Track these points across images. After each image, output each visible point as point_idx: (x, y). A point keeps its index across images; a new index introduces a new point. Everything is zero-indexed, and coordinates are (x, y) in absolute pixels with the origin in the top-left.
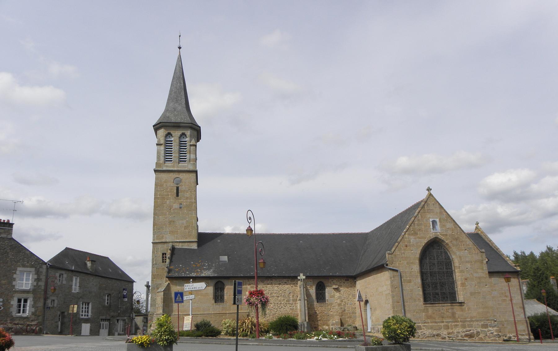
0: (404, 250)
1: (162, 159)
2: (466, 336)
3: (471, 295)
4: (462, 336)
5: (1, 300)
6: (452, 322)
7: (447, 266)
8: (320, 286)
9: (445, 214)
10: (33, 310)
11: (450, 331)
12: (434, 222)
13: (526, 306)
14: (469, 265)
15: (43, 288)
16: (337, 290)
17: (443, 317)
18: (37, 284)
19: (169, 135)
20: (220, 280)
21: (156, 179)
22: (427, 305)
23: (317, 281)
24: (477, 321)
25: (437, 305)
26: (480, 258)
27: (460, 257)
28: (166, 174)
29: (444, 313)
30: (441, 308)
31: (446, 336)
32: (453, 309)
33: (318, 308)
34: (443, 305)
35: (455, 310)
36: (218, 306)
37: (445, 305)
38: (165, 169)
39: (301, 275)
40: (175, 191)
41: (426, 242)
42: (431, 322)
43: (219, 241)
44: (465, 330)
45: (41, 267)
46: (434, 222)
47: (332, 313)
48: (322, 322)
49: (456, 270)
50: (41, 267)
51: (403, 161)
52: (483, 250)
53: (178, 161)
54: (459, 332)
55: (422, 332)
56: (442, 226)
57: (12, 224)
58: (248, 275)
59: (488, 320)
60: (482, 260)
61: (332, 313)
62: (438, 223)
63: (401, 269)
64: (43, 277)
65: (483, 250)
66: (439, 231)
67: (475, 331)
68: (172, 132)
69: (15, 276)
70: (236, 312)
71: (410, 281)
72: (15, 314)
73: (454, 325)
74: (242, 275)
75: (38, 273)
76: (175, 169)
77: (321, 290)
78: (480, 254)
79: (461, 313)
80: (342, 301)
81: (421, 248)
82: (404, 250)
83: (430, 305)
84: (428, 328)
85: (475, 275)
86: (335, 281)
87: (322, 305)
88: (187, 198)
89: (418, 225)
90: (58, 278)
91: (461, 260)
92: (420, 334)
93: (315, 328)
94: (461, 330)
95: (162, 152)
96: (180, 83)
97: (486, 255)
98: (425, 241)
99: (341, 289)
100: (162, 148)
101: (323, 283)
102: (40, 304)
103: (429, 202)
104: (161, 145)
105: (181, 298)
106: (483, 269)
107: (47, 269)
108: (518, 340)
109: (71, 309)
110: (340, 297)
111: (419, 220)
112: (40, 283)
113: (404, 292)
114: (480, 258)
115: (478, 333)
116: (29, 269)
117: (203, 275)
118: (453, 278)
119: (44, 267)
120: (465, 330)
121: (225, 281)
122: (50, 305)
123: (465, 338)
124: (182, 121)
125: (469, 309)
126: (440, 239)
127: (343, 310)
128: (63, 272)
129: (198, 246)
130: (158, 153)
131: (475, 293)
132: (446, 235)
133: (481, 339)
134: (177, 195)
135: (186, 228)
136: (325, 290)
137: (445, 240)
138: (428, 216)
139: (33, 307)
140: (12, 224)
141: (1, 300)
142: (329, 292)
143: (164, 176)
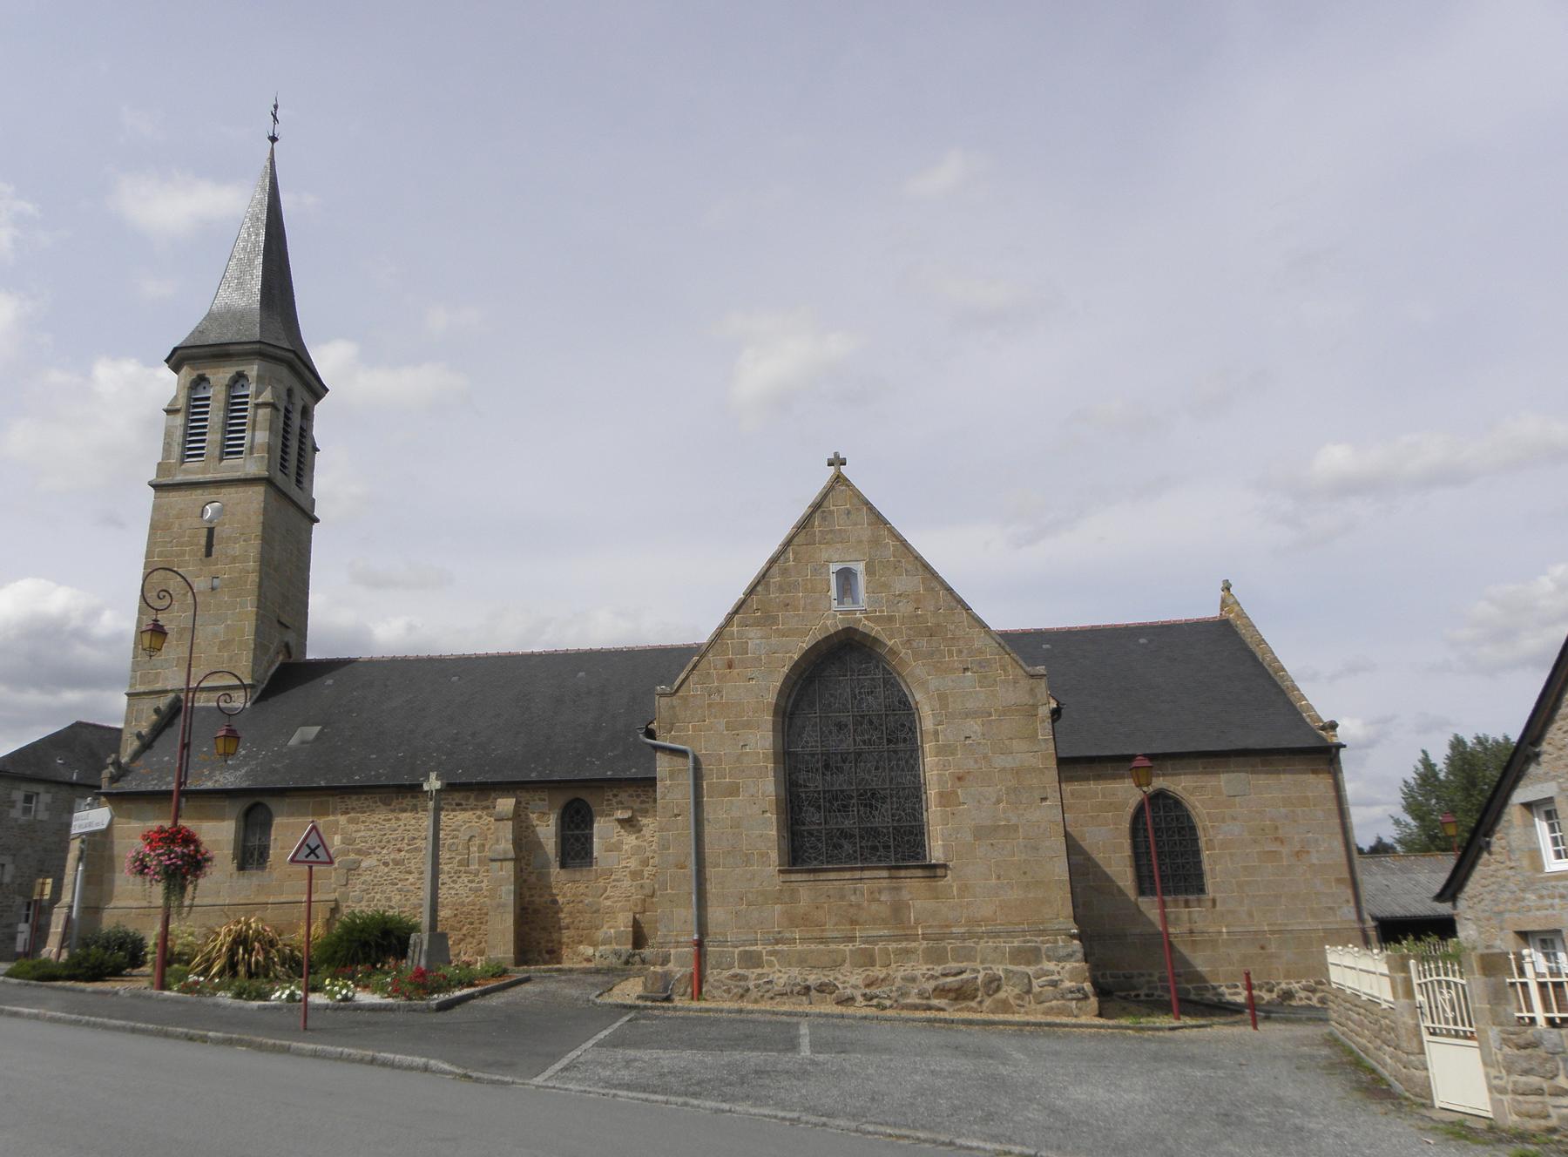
0: (722, 678)
1: (176, 450)
2: (941, 991)
3: (977, 838)
4: (921, 994)
6: (891, 939)
7: (897, 730)
8: (578, 812)
9: (892, 543)
12: (846, 576)
13: (1362, 877)
14: (975, 727)
16: (630, 824)
17: (853, 922)
19: (201, 381)
20: (258, 799)
21: (156, 508)
22: (793, 877)
23: (562, 799)
24: (996, 935)
25: (832, 876)
27: (942, 698)
28: (182, 493)
29: (859, 906)
30: (849, 886)
31: (858, 994)
32: (898, 889)
33: (564, 885)
34: (858, 874)
36: (244, 882)
37: (867, 874)
38: (179, 478)
39: (433, 776)
40: (203, 541)
41: (806, 646)
43: (330, 682)
44: (939, 969)
46: (846, 576)
47: (608, 903)
48: (572, 932)
49: (926, 746)
51: (1336, 458)
52: (1041, 669)
53: (217, 453)
54: (913, 979)
55: (760, 976)
58: (344, 782)
59: (1042, 932)
60: (1035, 706)
61: (608, 903)
62: (862, 580)
63: (700, 747)
65: (1041, 669)
66: (861, 608)
67: (981, 976)
68: (209, 374)
70: (305, 898)
71: (733, 791)
74: (323, 784)
76: (209, 477)
77: (578, 827)
78: (1025, 683)
79: (930, 904)
80: (645, 863)
82: (722, 678)
83: (805, 877)
84: (785, 959)
85: (1000, 761)
86: (623, 796)
87: (578, 876)
88: (234, 559)
89: (781, 589)
90: (20, 805)
92: (751, 985)
93: (551, 952)
94: (922, 969)
95: (179, 433)
96: (257, 235)
97: (1050, 687)
99: (644, 821)
100: (179, 420)
103: (830, 505)
104: (177, 411)
106: (1033, 737)
108: (1252, 1004)
109: (38, 889)
110: (637, 850)
111: (785, 572)
113: (708, 829)
115: (993, 984)
117: (209, 785)
118: (917, 776)
120: (939, 969)
121: (273, 804)
123: (935, 1002)
124: (237, 338)
126: (866, 636)
127: (648, 891)
128: (40, 788)
130: (168, 434)
131: (996, 828)
132: (891, 619)
133: (1004, 1006)
134: (209, 553)
135: (224, 645)
136: (589, 824)
137: (883, 637)
138: (825, 556)
142: (604, 830)
143: (175, 498)
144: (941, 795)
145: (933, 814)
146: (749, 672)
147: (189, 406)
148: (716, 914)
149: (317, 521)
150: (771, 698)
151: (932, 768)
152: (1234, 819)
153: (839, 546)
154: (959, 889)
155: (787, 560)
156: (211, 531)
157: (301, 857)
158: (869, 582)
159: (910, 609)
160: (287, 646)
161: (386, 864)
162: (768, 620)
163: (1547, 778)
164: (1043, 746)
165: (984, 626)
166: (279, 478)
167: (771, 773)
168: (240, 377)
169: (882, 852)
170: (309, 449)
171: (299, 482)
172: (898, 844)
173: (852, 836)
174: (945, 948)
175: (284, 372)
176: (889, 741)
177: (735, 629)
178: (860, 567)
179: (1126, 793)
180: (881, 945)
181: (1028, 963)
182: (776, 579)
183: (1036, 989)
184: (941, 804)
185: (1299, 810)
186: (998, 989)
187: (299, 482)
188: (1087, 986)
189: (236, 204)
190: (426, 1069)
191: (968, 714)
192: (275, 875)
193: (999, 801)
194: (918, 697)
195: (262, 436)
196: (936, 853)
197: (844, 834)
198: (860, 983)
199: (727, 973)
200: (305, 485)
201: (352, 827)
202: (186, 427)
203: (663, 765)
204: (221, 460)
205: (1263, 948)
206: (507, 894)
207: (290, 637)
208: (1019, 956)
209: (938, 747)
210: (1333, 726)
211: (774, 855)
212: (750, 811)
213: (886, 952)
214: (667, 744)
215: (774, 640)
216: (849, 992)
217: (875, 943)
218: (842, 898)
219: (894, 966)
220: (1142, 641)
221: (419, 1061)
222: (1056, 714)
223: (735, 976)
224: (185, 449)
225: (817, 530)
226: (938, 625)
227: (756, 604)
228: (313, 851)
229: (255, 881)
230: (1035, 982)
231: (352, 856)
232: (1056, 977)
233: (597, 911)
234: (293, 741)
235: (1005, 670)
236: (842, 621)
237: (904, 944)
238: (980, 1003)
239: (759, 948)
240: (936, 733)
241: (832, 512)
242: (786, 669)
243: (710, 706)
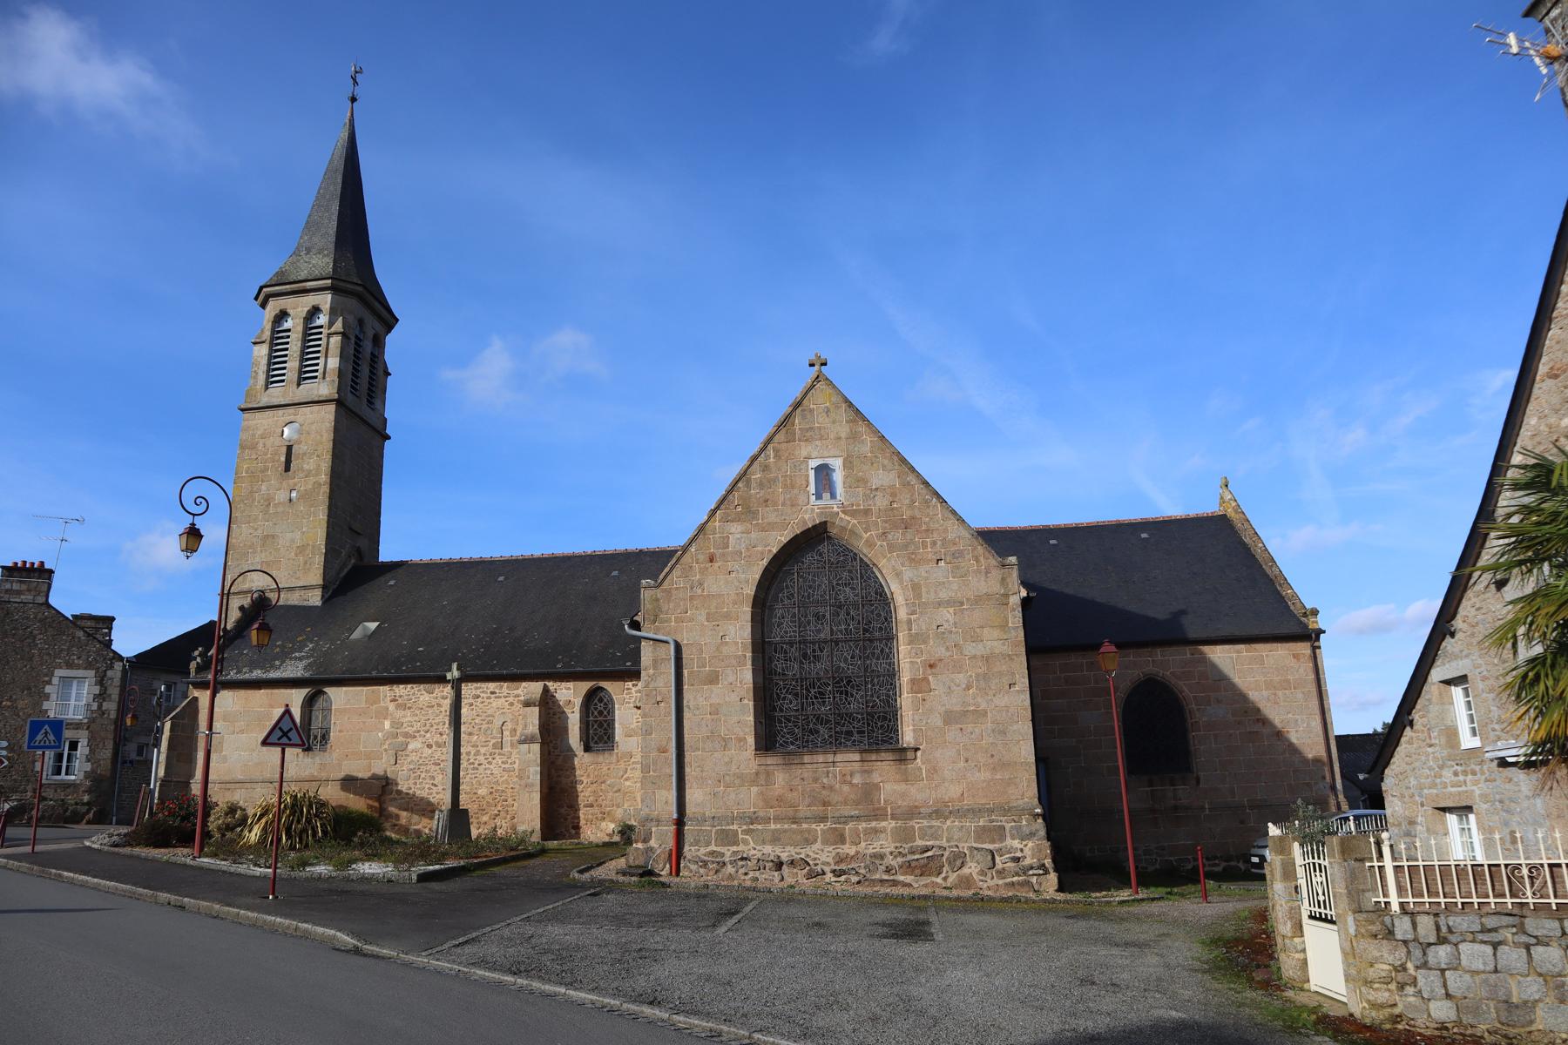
5: (5, 744)
10: (88, 767)
12: (823, 472)
14: (947, 615)
15: (113, 715)
18: (100, 707)
27: (916, 587)
29: (831, 788)
32: (869, 772)
35: (876, 778)
40: (283, 459)
41: (785, 540)
42: (777, 819)
45: (111, 667)
50: (111, 667)
52: (1013, 559)
54: (882, 857)
56: (854, 481)
57: (51, 572)
60: (1006, 596)
62: (838, 477)
64: (114, 692)
66: (837, 505)
67: (946, 854)
69: (48, 689)
71: (713, 679)
72: (47, 776)
73: (867, 832)
75: (101, 681)
78: (996, 574)
79: (902, 787)
81: (765, 563)
85: (971, 649)
87: (600, 758)
89: (761, 485)
91: (919, 596)
102: (106, 754)
105: (52, 737)
107: (124, 671)
111: (766, 468)
112: (105, 706)
113: (687, 715)
119: (118, 666)
122: (133, 756)
125: (933, 770)
129: (326, 600)
132: (867, 512)
134: (287, 469)
138: (804, 453)
140: (51, 572)
141: (5, 744)
144: (913, 681)
145: (906, 701)
147: (272, 339)
148: (694, 795)
152: (1219, 702)
154: (928, 771)
155: (768, 457)
156: (289, 448)
157: (273, 739)
158: (846, 477)
160: (359, 551)
161: (430, 746)
162: (749, 513)
163: (1455, 657)
164: (1013, 633)
165: (961, 520)
168: (315, 311)
169: (856, 737)
170: (381, 373)
171: (370, 403)
172: (876, 730)
173: (828, 721)
175: (352, 303)
176: (865, 631)
180: (850, 825)
182: (756, 476)
183: (999, 866)
184: (912, 691)
186: (963, 864)
187: (370, 403)
188: (1048, 862)
189: (323, 155)
190: (357, 951)
191: (940, 604)
192: (335, 755)
195: (333, 363)
197: (820, 720)
198: (830, 860)
199: (703, 850)
201: (400, 713)
203: (647, 653)
204: (299, 385)
206: (534, 774)
207: (363, 543)
210: (1315, 612)
211: (751, 740)
212: (727, 700)
214: (651, 635)
215: (753, 535)
216: (819, 868)
217: (845, 823)
218: (816, 780)
220: (1144, 535)
221: (349, 940)
222: (1025, 603)
224: (268, 376)
226: (913, 518)
227: (733, 501)
229: (318, 760)
230: (998, 859)
231: (401, 739)
232: (1019, 854)
234: (357, 634)
235: (977, 561)
237: (873, 824)
238: (945, 879)
240: (909, 622)
241: (812, 411)
243: (692, 598)
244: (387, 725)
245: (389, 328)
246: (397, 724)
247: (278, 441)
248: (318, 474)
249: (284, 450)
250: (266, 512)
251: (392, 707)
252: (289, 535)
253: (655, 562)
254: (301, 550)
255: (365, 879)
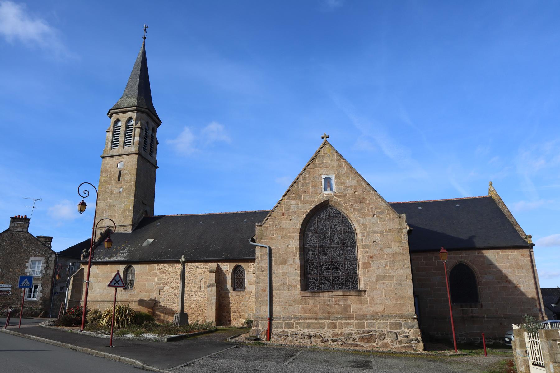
7: (347, 239)
10: (41, 295)
11: (338, 331)
12: (328, 180)
14: (377, 237)
15: (51, 275)
26: (397, 226)
27: (365, 226)
29: (331, 306)
31: (329, 339)
32: (346, 300)
40: (117, 176)
41: (312, 207)
42: (309, 318)
49: (359, 245)
54: (351, 334)
56: (340, 184)
60: (401, 229)
61: (250, 303)
62: (333, 182)
64: (52, 266)
69: (27, 265)
71: (284, 262)
72: (26, 299)
75: (47, 262)
78: (397, 220)
82: (280, 219)
85: (387, 250)
87: (239, 293)
88: (127, 182)
89: (303, 185)
91: (366, 229)
98: (312, 206)
101: (240, 266)
102: (48, 290)
105: (28, 283)
111: (305, 179)
112: (48, 271)
114: (397, 226)
116: (39, 258)
119: (54, 256)
122: (59, 291)
129: (133, 230)
132: (345, 196)
134: (119, 180)
138: (320, 173)
139: (41, 292)
144: (364, 263)
145: (361, 271)
146: (291, 217)
147: (114, 130)
148: (277, 308)
149: (158, 168)
150: (299, 227)
151: (361, 255)
152: (490, 273)
153: (325, 169)
154: (370, 300)
156: (120, 172)
158: (337, 182)
159: (353, 192)
160: (146, 211)
161: (173, 288)
162: (298, 196)
166: (143, 153)
167: (298, 255)
168: (130, 119)
169: (341, 286)
170: (155, 143)
172: (348, 283)
173: (329, 279)
174: (364, 323)
175: (144, 116)
176: (345, 243)
177: (286, 201)
178: (333, 177)
179: (233, 265)
181: (396, 329)
183: (399, 339)
184: (363, 267)
185: (516, 270)
186: (384, 338)
187: (151, 154)
188: (419, 338)
189: (134, 59)
190: (143, 368)
192: (136, 291)
193: (386, 266)
194: (356, 226)
195: (137, 139)
196: (362, 286)
199: (280, 331)
200: (154, 155)
201: (161, 275)
202: (113, 137)
203: (258, 251)
204: (124, 147)
205: (501, 324)
207: (148, 208)
208: (392, 325)
209: (362, 245)
210: (530, 237)
212: (290, 271)
213: (341, 324)
215: (300, 205)
216: (326, 339)
217: (337, 320)
219: (344, 329)
223: (283, 332)
224: (112, 144)
225: (317, 162)
226: (363, 198)
227: (292, 192)
228: (117, 282)
229: (129, 293)
230: (399, 336)
231: (161, 285)
232: (407, 334)
233: (246, 306)
234: (145, 244)
235: (389, 215)
236: (326, 197)
237: (348, 321)
238: (377, 344)
239: (292, 321)
240: (362, 240)
241: (323, 156)
242: (304, 216)
243: (276, 230)
244: (156, 279)
245: (158, 125)
246: (160, 279)
247: (116, 169)
248: (131, 182)
249: (118, 172)
250: (111, 196)
251: (158, 272)
252: (119, 206)
253: (261, 216)
254: (124, 211)
255: (147, 340)
